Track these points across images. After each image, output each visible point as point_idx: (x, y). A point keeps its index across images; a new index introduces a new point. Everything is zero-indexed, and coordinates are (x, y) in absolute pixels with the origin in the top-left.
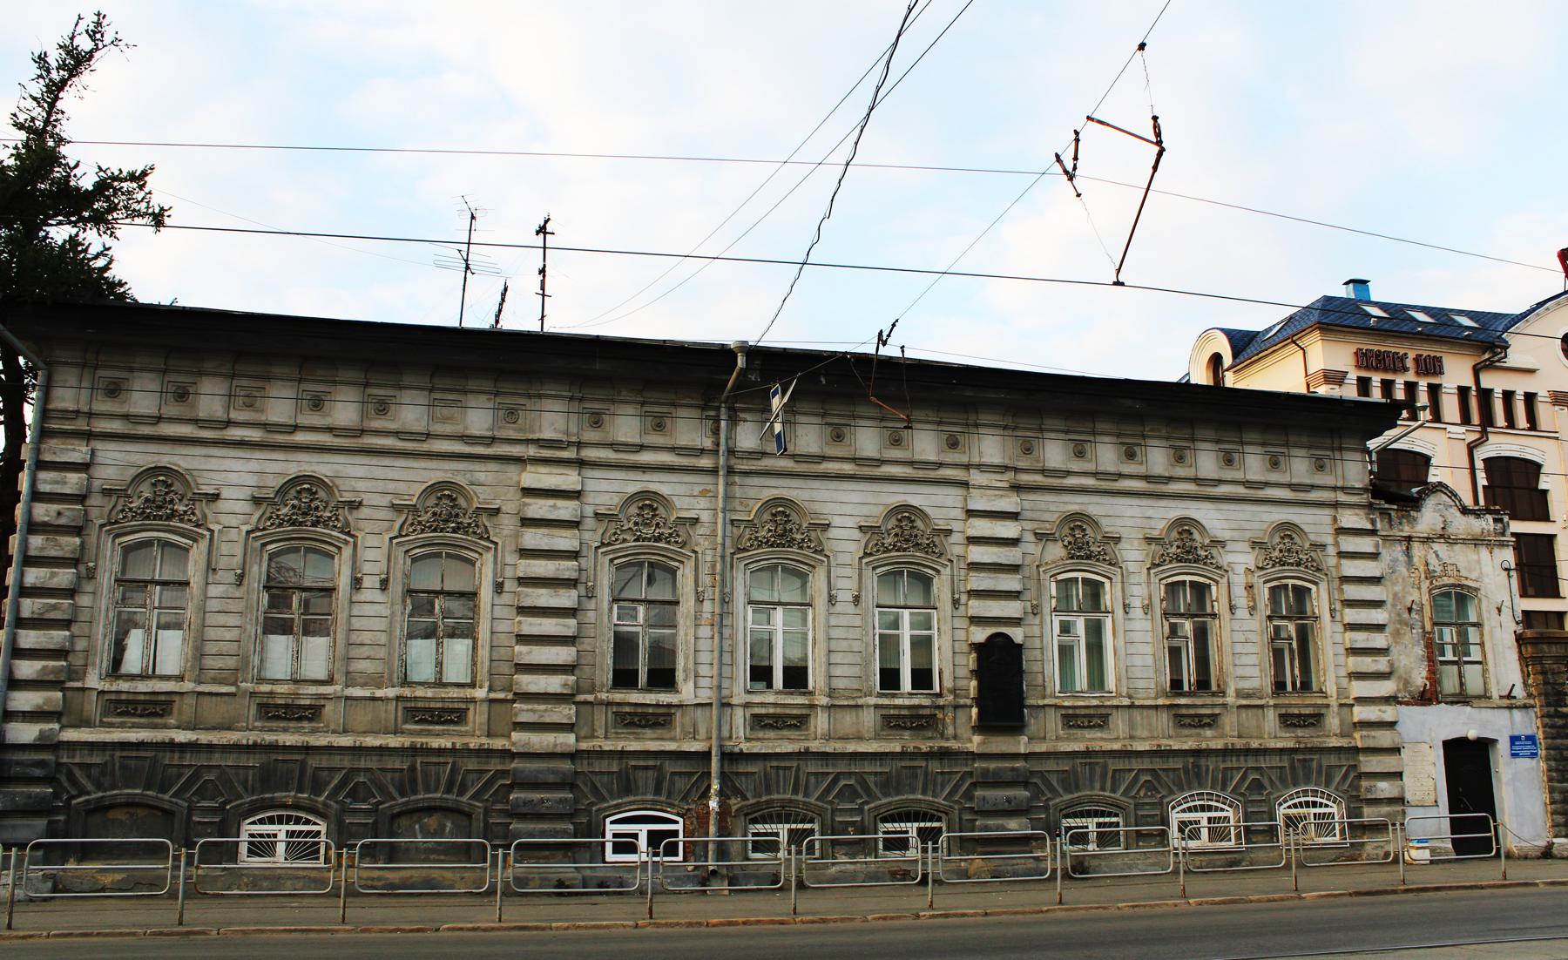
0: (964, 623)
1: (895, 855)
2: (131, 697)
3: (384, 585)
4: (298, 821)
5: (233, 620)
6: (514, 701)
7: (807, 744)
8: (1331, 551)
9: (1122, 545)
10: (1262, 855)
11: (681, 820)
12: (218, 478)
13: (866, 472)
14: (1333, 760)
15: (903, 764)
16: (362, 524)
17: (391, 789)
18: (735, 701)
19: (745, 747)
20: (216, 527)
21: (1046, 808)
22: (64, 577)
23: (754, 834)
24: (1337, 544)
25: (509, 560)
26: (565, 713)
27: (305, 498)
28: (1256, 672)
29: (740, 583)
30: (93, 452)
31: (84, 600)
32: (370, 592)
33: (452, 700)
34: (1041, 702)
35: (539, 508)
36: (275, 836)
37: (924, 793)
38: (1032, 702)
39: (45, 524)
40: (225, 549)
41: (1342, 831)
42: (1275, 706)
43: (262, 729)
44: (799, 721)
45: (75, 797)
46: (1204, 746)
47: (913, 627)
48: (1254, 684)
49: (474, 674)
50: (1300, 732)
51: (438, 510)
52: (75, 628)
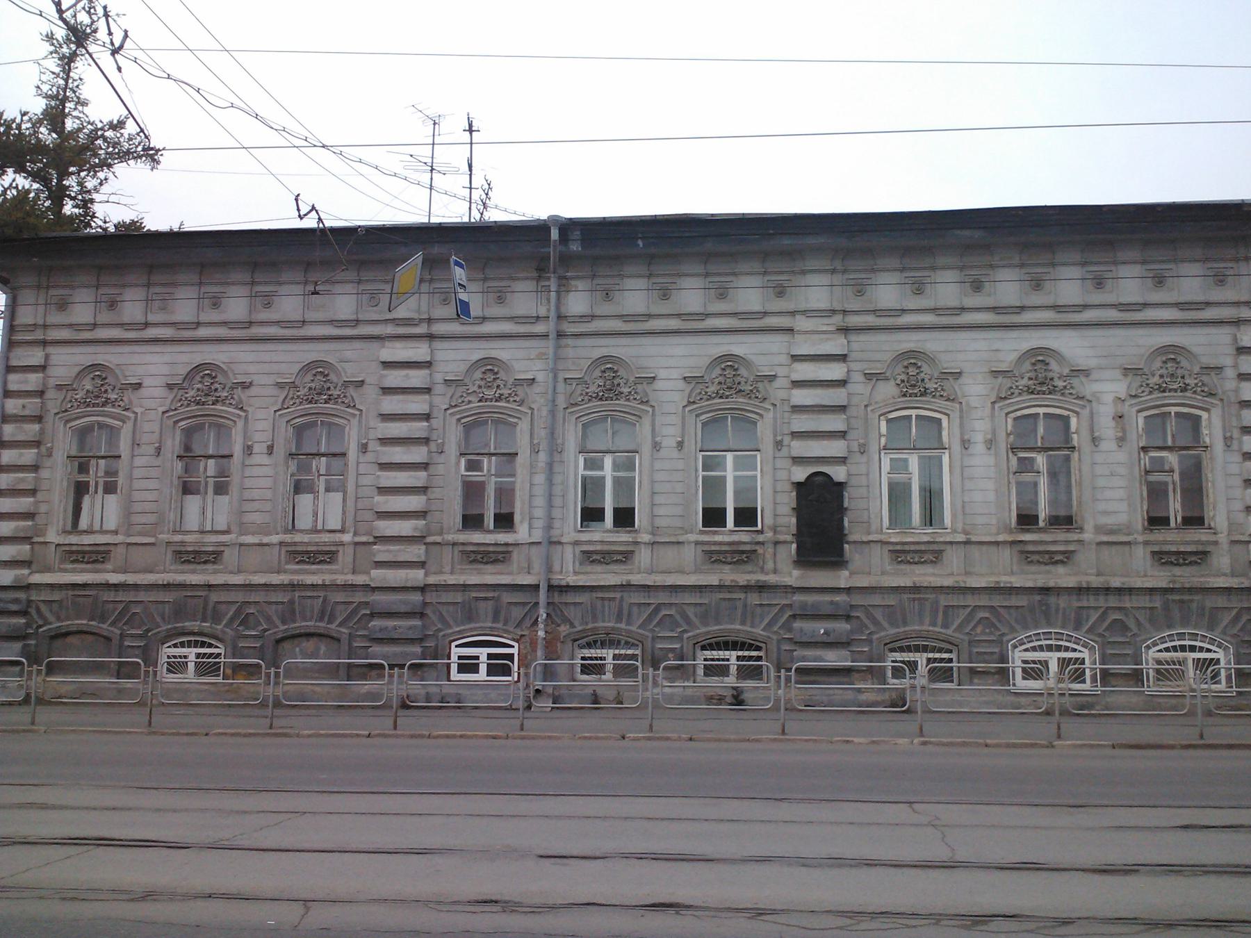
0: (787, 463)
1: (714, 681)
2: (79, 548)
3: (270, 450)
4: (203, 644)
5: (152, 484)
6: (375, 543)
7: (630, 577)
8: (1230, 373)
9: (964, 379)
10: (1122, 699)
11: (516, 645)
12: (140, 370)
13: (692, 326)
14: (1221, 601)
15: (722, 596)
16: (253, 401)
17: (275, 618)
18: (564, 540)
19: (572, 580)
20: (138, 410)
21: (869, 641)
22: (28, 456)
23: (583, 658)
24: (1235, 366)
25: (372, 424)
26: (415, 552)
27: (208, 381)
28: (1123, 507)
29: (571, 436)
30: (47, 357)
31: (44, 473)
32: (260, 458)
33: (325, 544)
34: (865, 539)
35: (395, 378)
36: (185, 657)
37: (743, 623)
38: (851, 538)
39: (16, 416)
40: (147, 427)
41: (1229, 678)
42: (1146, 543)
43: (176, 572)
44: (626, 556)
45: (41, 626)
46: (1051, 584)
47: (736, 469)
48: (1122, 518)
49: (344, 522)
50: (1177, 571)
51: (313, 385)
52: (40, 496)
